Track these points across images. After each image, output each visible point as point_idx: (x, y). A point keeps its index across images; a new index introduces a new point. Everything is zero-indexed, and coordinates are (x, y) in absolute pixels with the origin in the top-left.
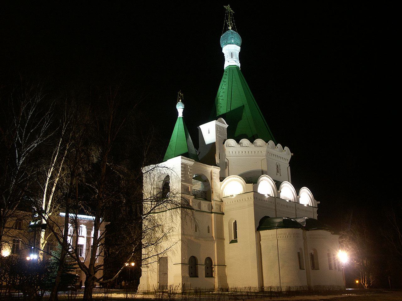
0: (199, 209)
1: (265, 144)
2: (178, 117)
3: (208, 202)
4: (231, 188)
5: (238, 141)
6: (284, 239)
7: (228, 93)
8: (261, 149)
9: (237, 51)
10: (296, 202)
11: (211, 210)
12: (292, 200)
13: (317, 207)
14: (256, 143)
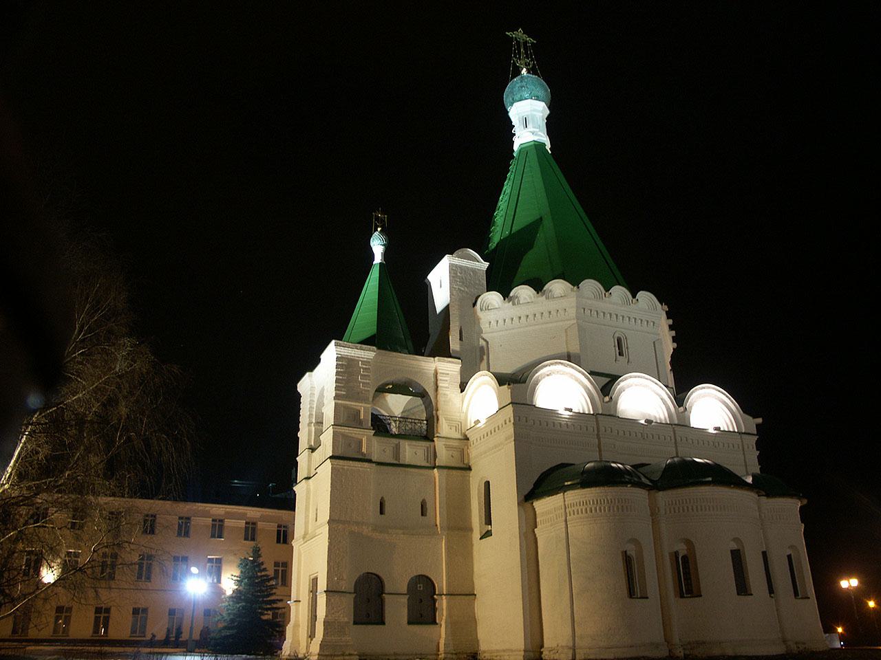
0: (396, 460)
1: (572, 290)
2: (374, 263)
3: (427, 444)
4: (475, 404)
5: (506, 294)
6: (581, 518)
7: (517, 203)
8: (564, 303)
9: (538, 111)
10: (676, 422)
11: (432, 461)
12: (663, 417)
13: (755, 432)
14: (551, 291)
